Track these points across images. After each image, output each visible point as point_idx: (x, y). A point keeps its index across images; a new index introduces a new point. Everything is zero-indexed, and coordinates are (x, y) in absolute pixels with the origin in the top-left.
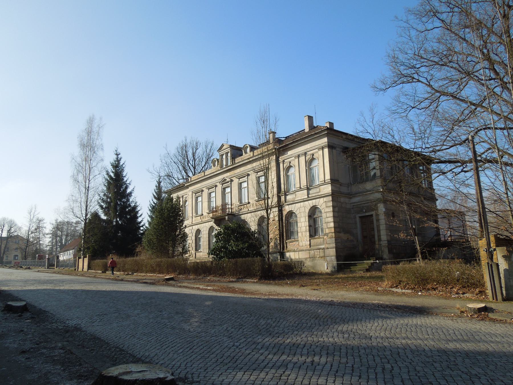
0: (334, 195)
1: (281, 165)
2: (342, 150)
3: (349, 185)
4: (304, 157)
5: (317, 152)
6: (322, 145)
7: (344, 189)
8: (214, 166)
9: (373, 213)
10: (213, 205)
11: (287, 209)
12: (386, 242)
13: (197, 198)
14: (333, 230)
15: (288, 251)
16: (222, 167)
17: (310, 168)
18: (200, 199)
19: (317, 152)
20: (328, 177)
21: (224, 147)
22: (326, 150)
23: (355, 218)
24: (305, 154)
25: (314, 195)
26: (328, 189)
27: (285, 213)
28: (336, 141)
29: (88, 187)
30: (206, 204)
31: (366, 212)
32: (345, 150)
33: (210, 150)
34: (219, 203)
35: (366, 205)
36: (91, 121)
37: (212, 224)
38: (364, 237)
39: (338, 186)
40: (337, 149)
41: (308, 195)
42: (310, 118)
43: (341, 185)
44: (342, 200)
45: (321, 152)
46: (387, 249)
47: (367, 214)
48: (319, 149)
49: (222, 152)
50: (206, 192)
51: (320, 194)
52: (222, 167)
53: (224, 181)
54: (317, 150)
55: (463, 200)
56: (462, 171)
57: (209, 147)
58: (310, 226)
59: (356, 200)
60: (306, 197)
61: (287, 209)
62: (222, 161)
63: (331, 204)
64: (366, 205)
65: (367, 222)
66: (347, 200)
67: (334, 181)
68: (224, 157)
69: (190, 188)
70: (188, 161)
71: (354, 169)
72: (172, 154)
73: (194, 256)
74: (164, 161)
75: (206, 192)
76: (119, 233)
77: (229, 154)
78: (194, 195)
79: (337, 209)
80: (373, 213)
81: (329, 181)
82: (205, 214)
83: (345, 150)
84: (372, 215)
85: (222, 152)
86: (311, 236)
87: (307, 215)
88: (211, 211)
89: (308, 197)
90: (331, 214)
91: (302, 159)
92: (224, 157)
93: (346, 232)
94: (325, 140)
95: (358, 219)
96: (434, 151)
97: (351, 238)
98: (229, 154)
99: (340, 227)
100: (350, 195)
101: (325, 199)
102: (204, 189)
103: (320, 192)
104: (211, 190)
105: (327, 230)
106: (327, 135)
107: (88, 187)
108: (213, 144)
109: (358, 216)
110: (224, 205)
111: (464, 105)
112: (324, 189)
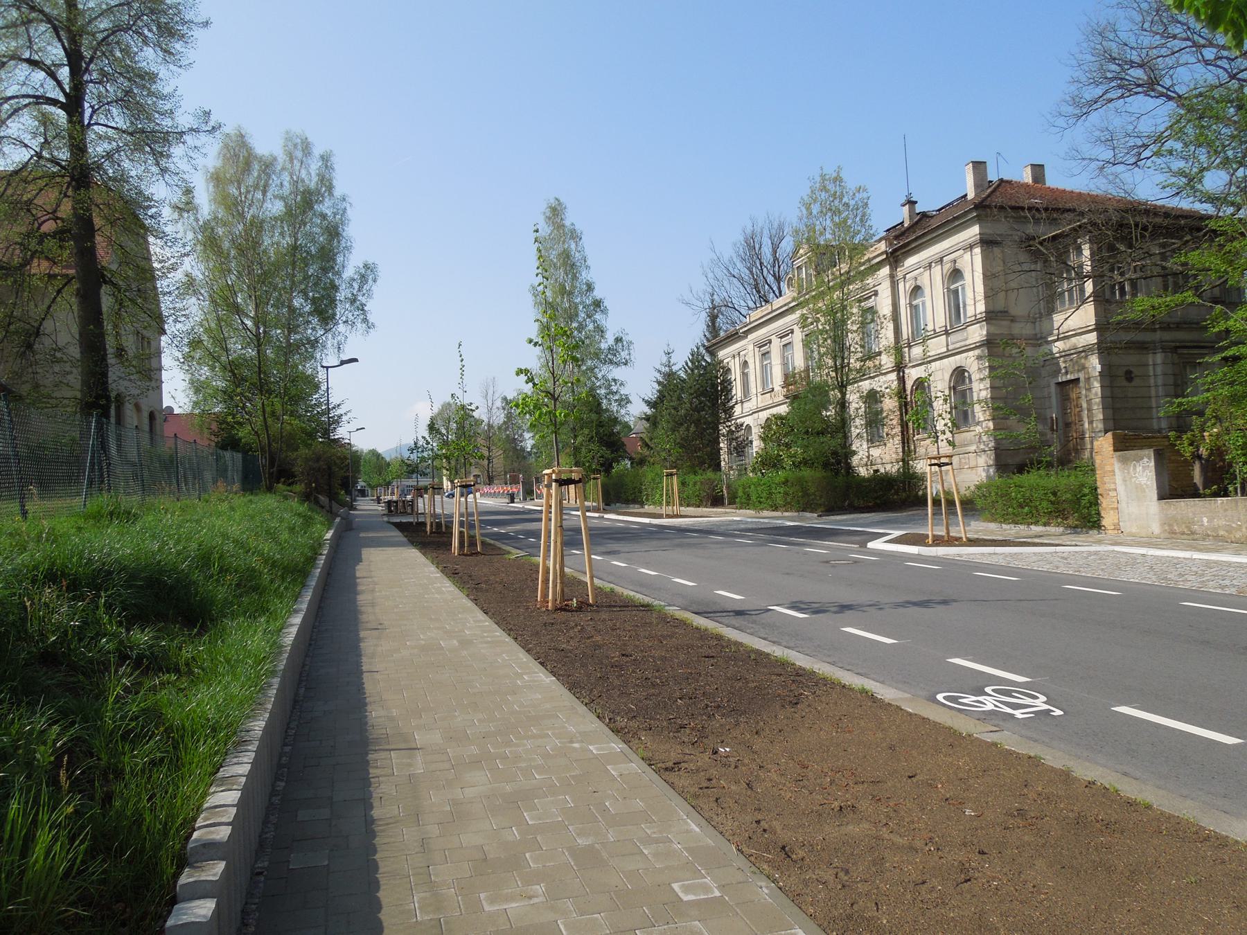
1: (901, 286)
5: (961, 256)
11: (913, 374)
19: (920, 274)
22: (977, 250)
24: (941, 260)
25: (958, 345)
27: (909, 385)
28: (1001, 227)
36: (556, 212)
42: (979, 166)
45: (967, 256)
51: (968, 342)
54: (961, 252)
57: (767, 251)
61: (913, 374)
69: (750, 337)
70: (761, 264)
72: (726, 259)
74: (710, 275)
76: (827, 410)
82: (777, 388)
84: (1078, 379)
88: (789, 379)
91: (937, 270)
94: (975, 229)
96: (250, 501)
99: (1003, 406)
101: (977, 352)
106: (979, 219)
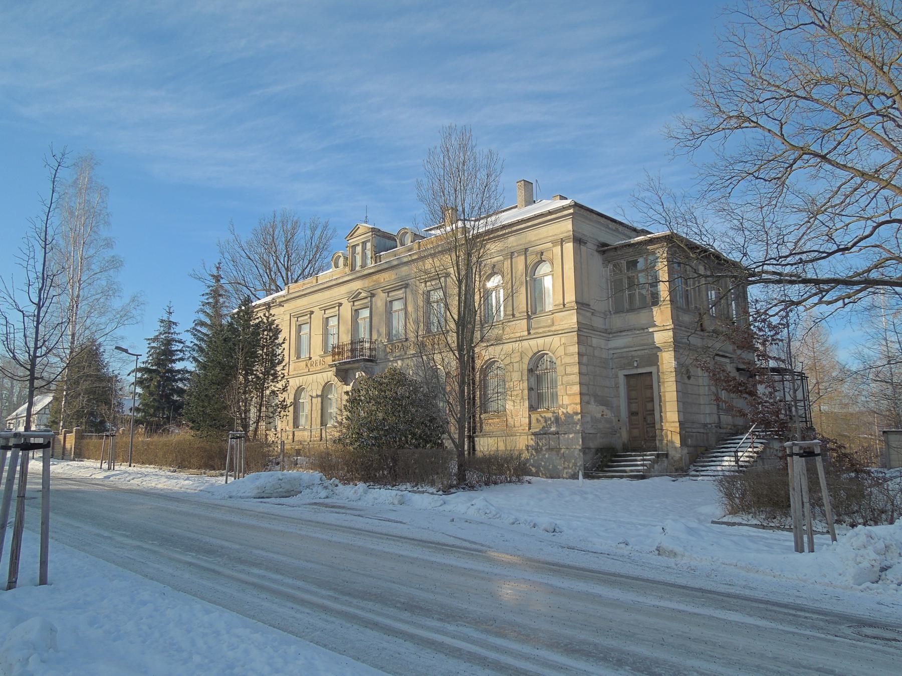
0: (583, 332)
2: (596, 247)
3: (606, 315)
4: (523, 257)
6: (562, 236)
7: (598, 322)
8: (337, 267)
9: (652, 369)
10: (333, 341)
12: (678, 425)
13: (299, 328)
14: (578, 400)
15: (484, 436)
16: (353, 269)
17: (535, 280)
18: (305, 329)
20: (571, 297)
21: (359, 232)
22: (569, 247)
23: (617, 376)
26: (571, 320)
28: (593, 231)
29: (78, 296)
30: (317, 341)
31: (637, 367)
32: (604, 249)
33: (321, 238)
34: (346, 339)
35: (639, 353)
37: (330, 375)
38: (633, 414)
39: (589, 314)
40: (589, 245)
41: (529, 330)
43: (593, 314)
44: (595, 341)
46: (678, 437)
47: (640, 371)
48: (554, 243)
49: (353, 242)
50: (318, 316)
51: (553, 328)
52: (353, 269)
53: (355, 297)
55: (245, 393)
56: (820, 302)
57: (318, 233)
58: (530, 389)
59: (618, 342)
60: (526, 333)
62: (354, 258)
63: (575, 349)
64: (639, 353)
65: (642, 386)
66: (602, 343)
67: (582, 305)
68: (359, 249)
71: (617, 287)
73: (291, 437)
75: (318, 316)
77: (369, 245)
78: (294, 320)
79: (585, 359)
80: (652, 369)
81: (574, 304)
83: (604, 249)
85: (353, 242)
86: (532, 408)
87: (525, 367)
89: (529, 333)
90: (576, 369)
92: (359, 249)
93: (603, 402)
95: (622, 380)
97: (609, 414)
98: (369, 245)
100: (609, 333)
102: (316, 309)
103: (553, 324)
104: (329, 313)
105: (566, 398)
107: (78, 296)
108: (326, 227)
109: (621, 374)
110: (355, 342)
111: (844, 175)
112: (561, 320)
